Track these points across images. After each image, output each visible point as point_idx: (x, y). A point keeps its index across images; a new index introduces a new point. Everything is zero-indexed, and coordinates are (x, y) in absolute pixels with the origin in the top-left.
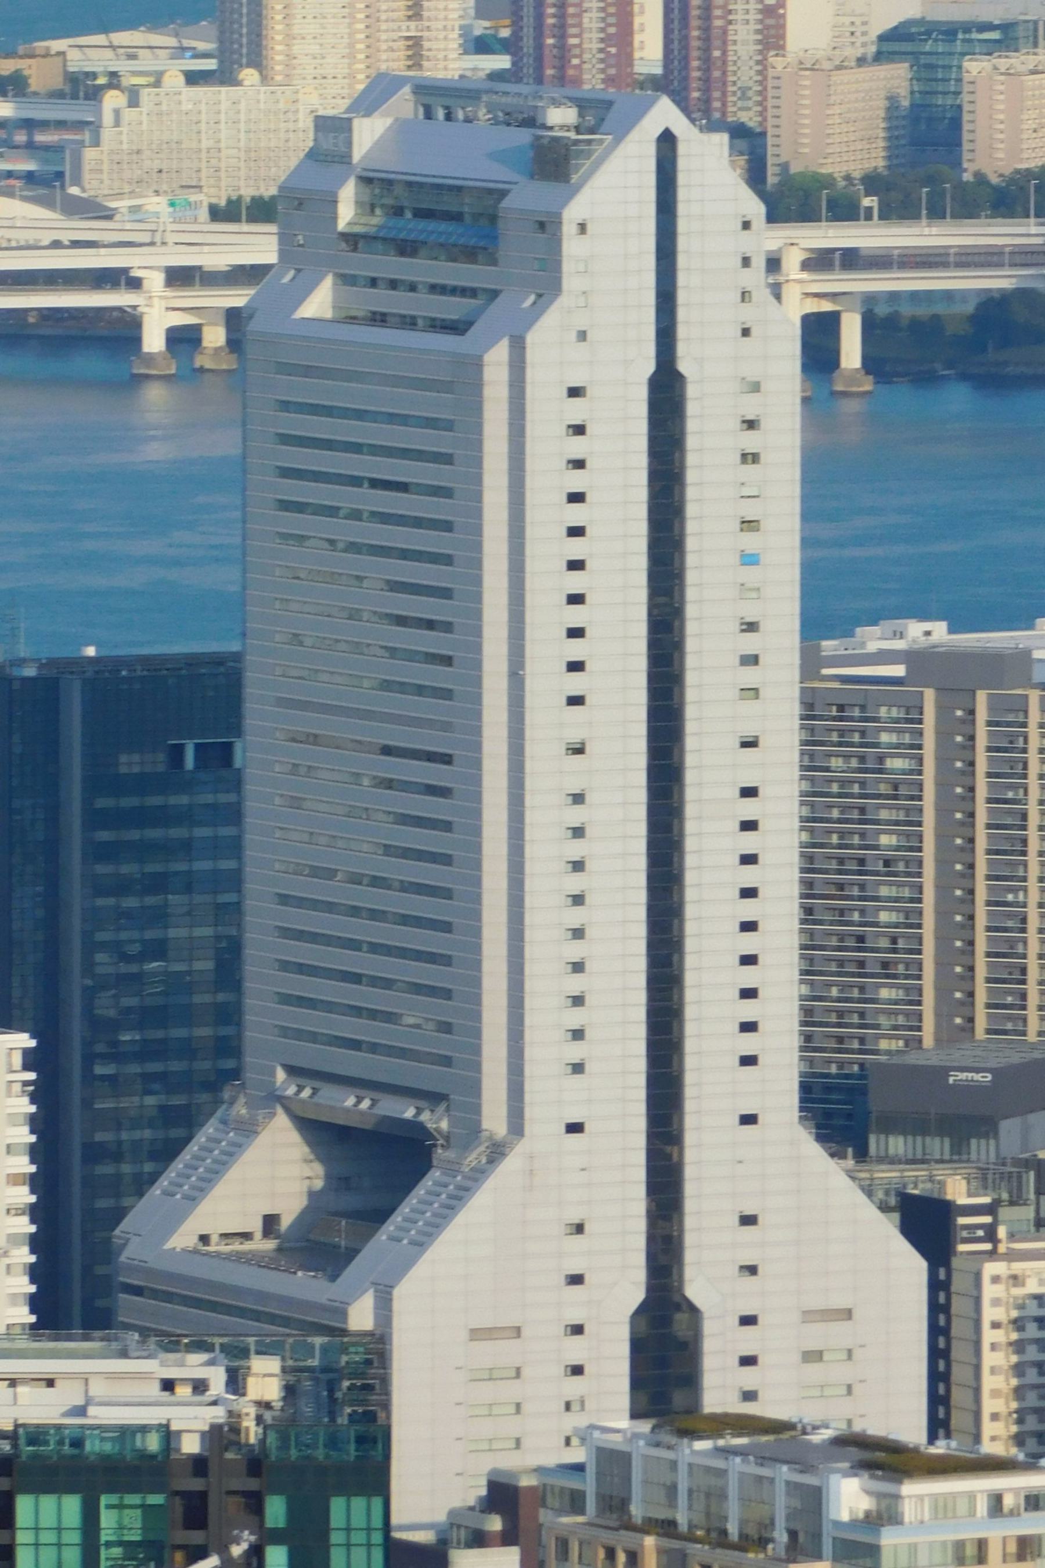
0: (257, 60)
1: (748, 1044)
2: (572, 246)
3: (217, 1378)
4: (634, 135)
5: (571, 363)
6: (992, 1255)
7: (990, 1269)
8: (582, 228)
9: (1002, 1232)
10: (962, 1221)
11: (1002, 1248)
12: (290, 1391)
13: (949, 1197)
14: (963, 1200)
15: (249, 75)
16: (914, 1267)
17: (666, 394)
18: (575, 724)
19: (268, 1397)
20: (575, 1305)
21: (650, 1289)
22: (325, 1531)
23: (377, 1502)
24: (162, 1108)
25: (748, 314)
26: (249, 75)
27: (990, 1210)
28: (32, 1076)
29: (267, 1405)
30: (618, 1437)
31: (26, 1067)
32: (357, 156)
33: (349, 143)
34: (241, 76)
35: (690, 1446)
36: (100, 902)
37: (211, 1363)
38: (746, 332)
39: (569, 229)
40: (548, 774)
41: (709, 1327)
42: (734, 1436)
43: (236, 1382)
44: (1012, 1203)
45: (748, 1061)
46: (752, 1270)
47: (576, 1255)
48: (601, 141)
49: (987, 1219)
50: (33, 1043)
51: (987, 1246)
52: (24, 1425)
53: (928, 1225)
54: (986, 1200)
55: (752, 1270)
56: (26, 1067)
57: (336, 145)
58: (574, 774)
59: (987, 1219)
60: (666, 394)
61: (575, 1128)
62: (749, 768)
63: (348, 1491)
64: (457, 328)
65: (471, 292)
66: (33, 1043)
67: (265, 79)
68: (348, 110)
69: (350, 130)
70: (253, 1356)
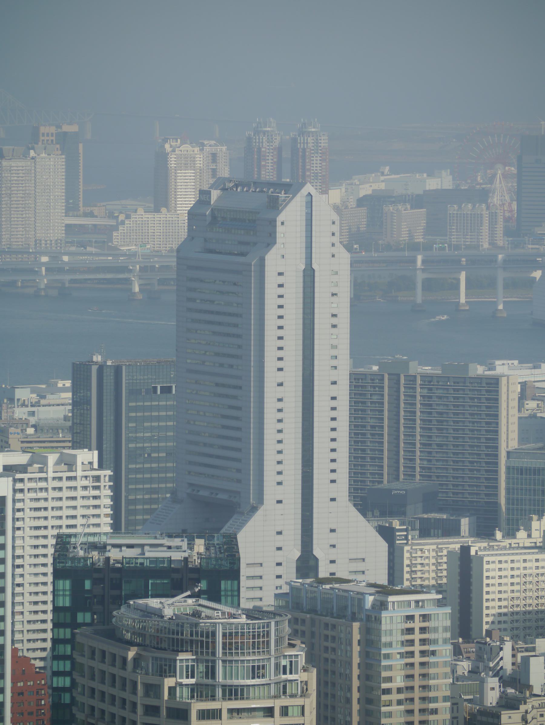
0: (167, 206)
1: (333, 476)
2: (280, 229)
3: (184, 545)
4: (299, 195)
5: (282, 263)
6: (407, 544)
7: (406, 548)
8: (283, 223)
9: (410, 537)
10: (397, 534)
11: (410, 542)
12: (207, 549)
13: (394, 526)
14: (398, 527)
15: (164, 210)
16: (384, 546)
17: (309, 275)
18: (280, 377)
19: (200, 551)
20: (279, 557)
21: (302, 552)
22: (220, 590)
23: (236, 582)
24: (151, 499)
25: (334, 250)
26: (164, 210)
27: (406, 530)
28: (112, 484)
29: (201, 554)
30: (299, 584)
31: (110, 481)
32: (212, 203)
33: (210, 198)
34: (161, 210)
35: (322, 587)
36: (130, 435)
37: (183, 541)
38: (333, 256)
39: (278, 223)
40: (271, 392)
41: (321, 564)
42: (335, 584)
43: (191, 547)
44: (412, 530)
45: (333, 481)
46: (334, 546)
47: (279, 541)
48: (289, 197)
49: (405, 533)
50: (112, 473)
51: (405, 542)
52: (126, 558)
53: (387, 533)
54: (405, 527)
55: (334, 546)
56: (110, 481)
57: (206, 199)
58: (280, 392)
59: (405, 533)
60: (309, 275)
61: (279, 502)
62: (334, 391)
63: (227, 578)
64: (243, 254)
65: (247, 243)
66: (112, 473)
67: (168, 211)
68: (209, 188)
69: (210, 194)
70: (196, 540)
